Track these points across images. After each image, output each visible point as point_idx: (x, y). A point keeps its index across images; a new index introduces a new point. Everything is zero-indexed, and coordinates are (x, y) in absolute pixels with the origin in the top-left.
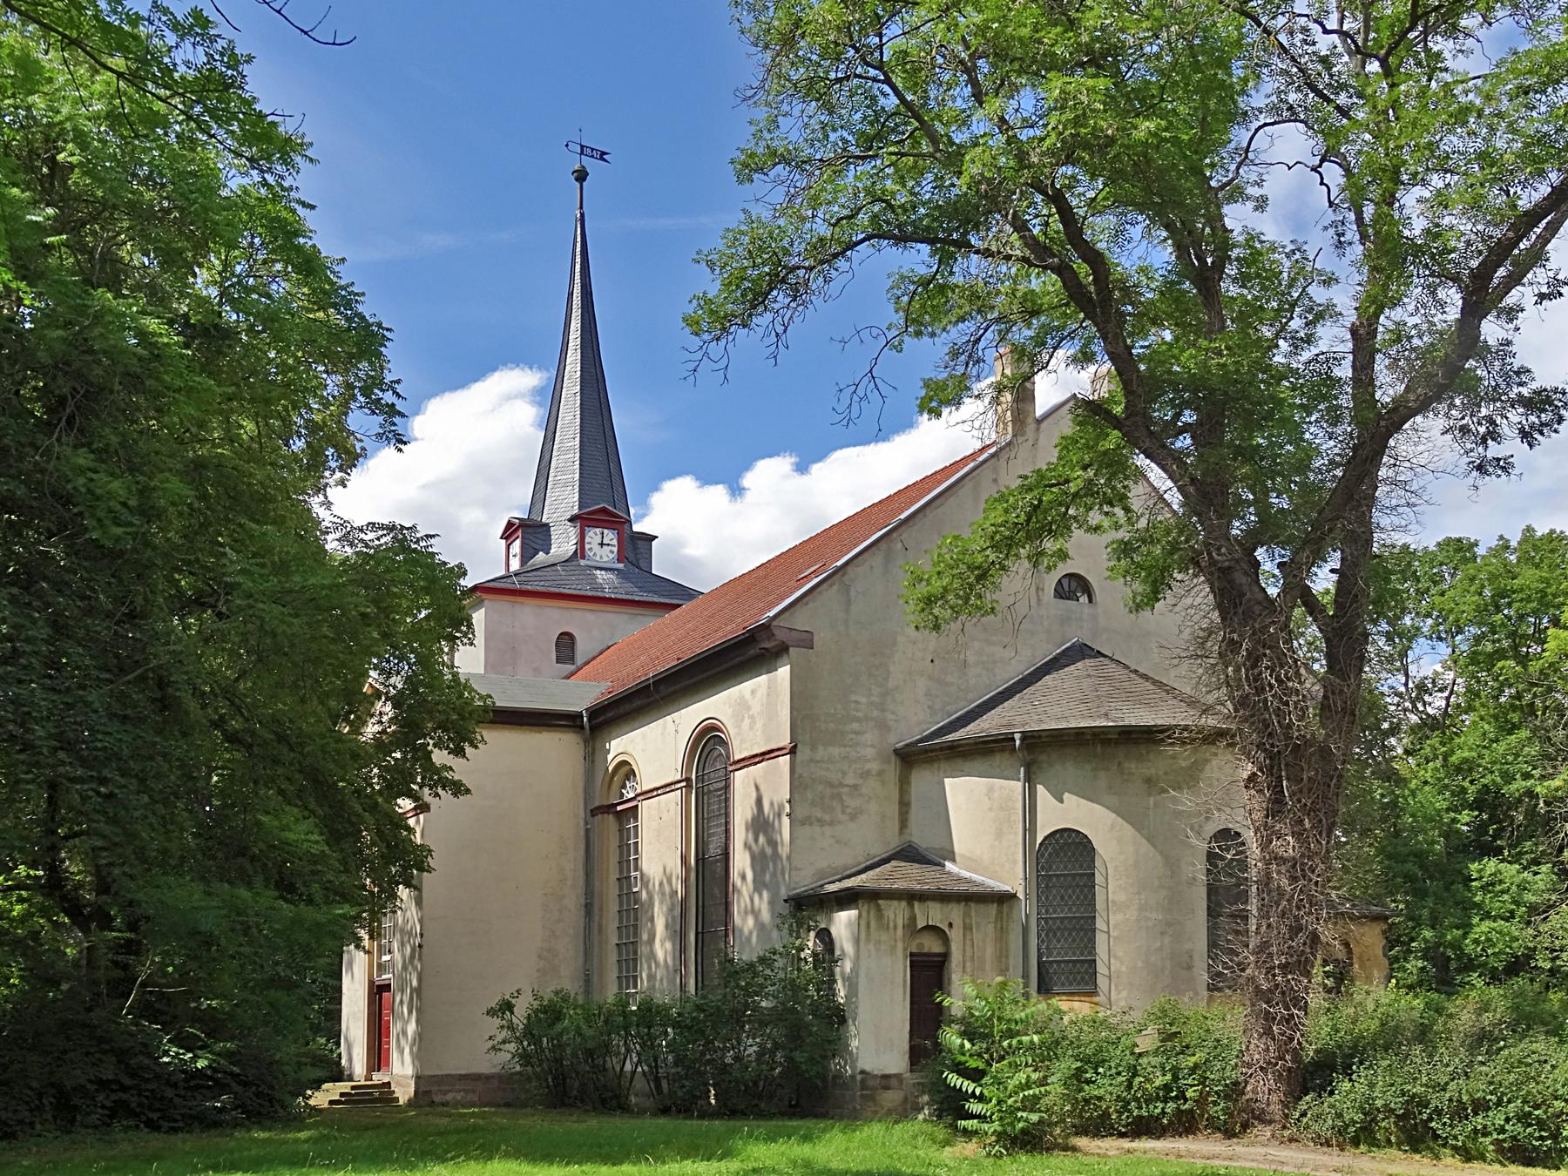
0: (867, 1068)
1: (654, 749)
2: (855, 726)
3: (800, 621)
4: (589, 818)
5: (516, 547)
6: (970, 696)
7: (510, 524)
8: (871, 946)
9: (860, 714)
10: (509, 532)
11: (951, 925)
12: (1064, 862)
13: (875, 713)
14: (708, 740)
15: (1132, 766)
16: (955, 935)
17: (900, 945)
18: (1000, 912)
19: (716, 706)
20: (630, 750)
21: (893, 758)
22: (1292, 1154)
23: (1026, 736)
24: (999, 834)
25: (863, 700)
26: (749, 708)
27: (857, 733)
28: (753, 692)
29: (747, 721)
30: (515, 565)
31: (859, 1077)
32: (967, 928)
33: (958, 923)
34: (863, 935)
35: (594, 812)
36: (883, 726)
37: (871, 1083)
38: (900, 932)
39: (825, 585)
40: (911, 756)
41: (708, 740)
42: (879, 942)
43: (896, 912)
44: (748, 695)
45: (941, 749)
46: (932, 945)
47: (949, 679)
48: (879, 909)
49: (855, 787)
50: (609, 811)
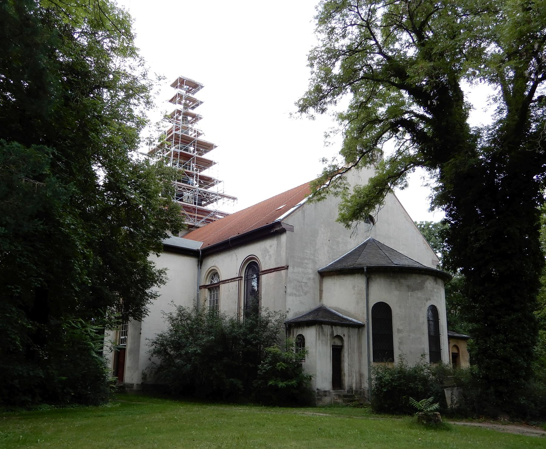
0: (319, 387)
2: (306, 261)
3: (290, 222)
4: (199, 290)
6: (340, 254)
8: (320, 342)
9: (308, 257)
12: (382, 314)
13: (312, 257)
15: (403, 281)
16: (345, 339)
17: (329, 342)
18: (359, 331)
19: (254, 250)
20: (217, 265)
21: (318, 274)
22: (491, 426)
23: (368, 268)
24: (358, 303)
25: (309, 252)
26: (269, 252)
27: (307, 264)
28: (271, 246)
29: (267, 257)
31: (317, 391)
32: (349, 337)
33: (346, 334)
34: (318, 338)
35: (201, 287)
36: (314, 262)
37: (321, 394)
38: (329, 337)
39: (297, 210)
40: (324, 274)
42: (322, 340)
43: (327, 329)
44: (268, 247)
46: (338, 343)
47: (334, 247)
48: (322, 328)
49: (306, 283)
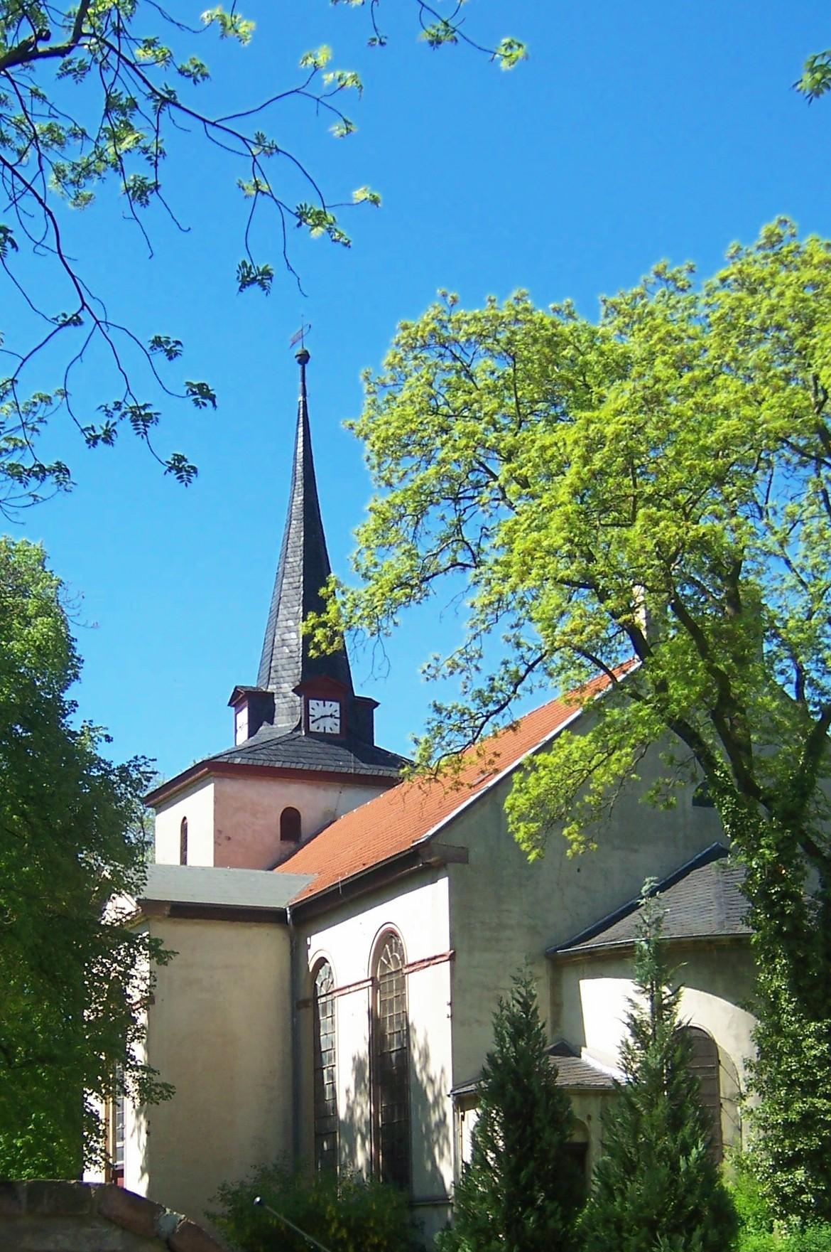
1: (343, 947)
3: (456, 839)
5: (243, 716)
7: (236, 692)
10: (237, 699)
11: (589, 1118)
14: (388, 939)
30: (243, 737)
41: (388, 939)
45: (583, 954)
50: (304, 1000)
